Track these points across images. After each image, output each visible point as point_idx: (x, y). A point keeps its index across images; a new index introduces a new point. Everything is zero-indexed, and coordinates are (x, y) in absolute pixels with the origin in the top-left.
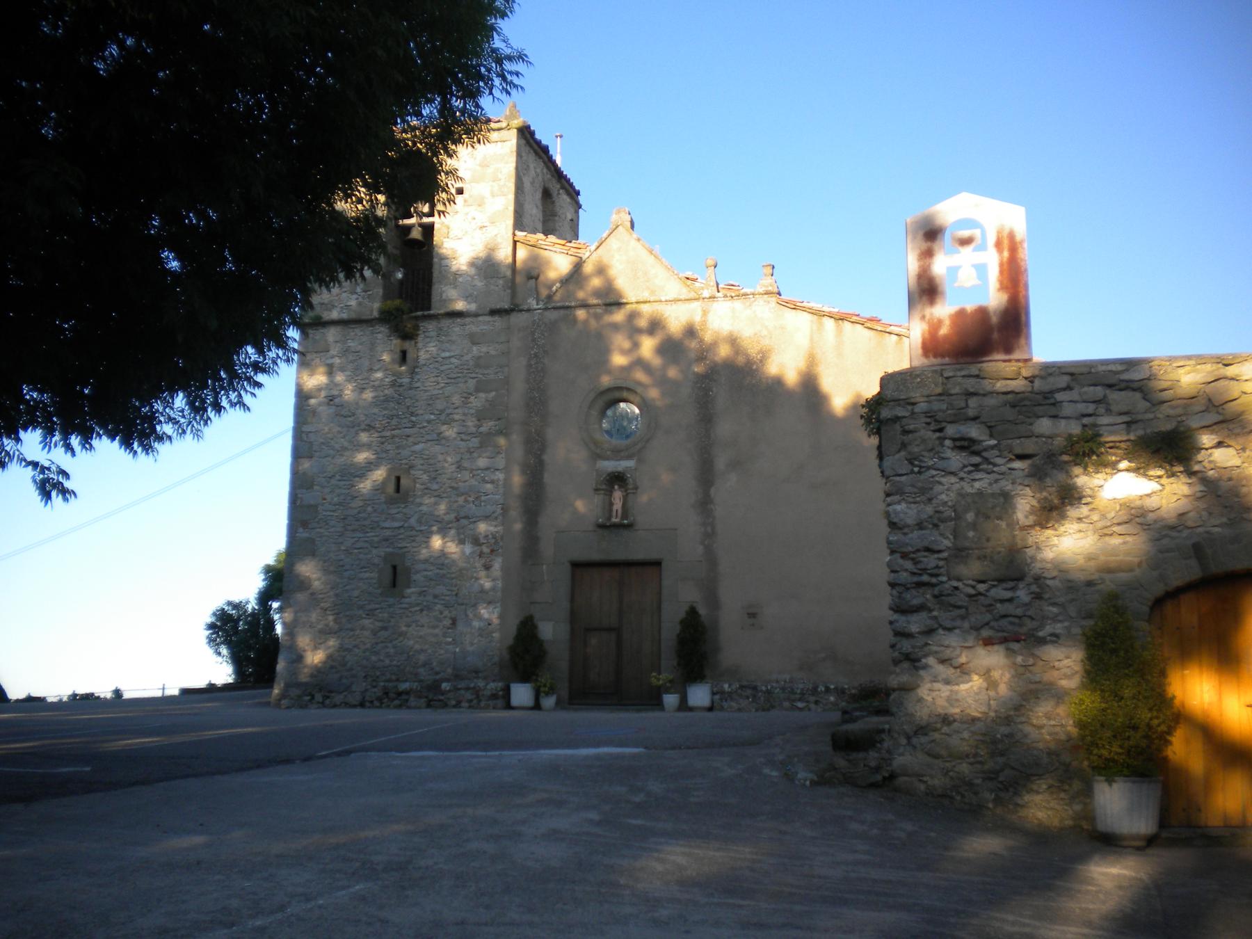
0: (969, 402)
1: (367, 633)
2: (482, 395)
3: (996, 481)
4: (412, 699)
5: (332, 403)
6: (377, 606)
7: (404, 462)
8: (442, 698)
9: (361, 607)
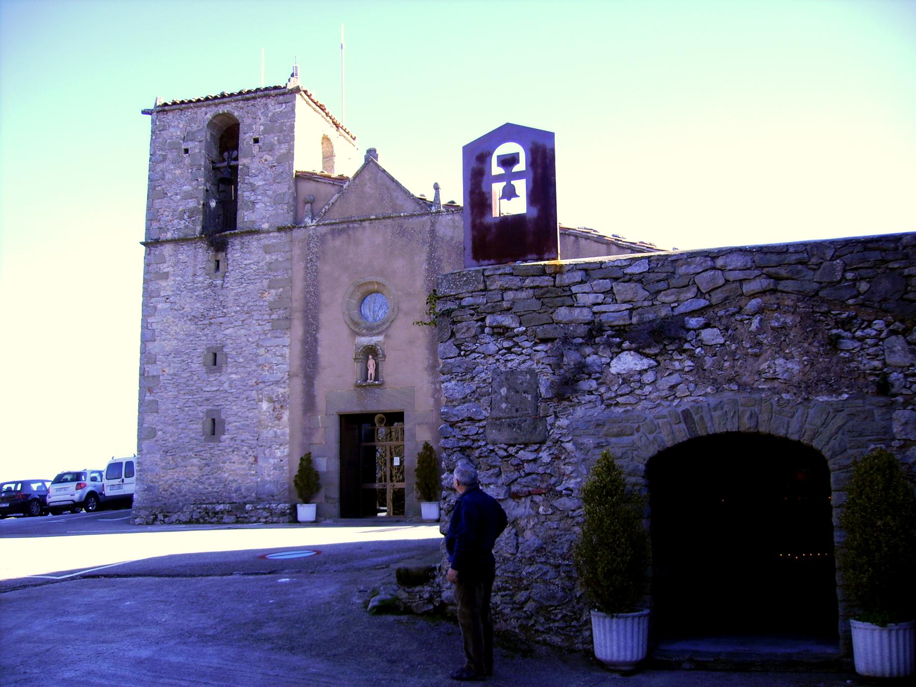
0: (504, 295)
1: (195, 468)
2: (273, 291)
3: (524, 362)
4: (225, 516)
5: (168, 300)
6: (203, 449)
7: (218, 342)
8: (246, 515)
9: (190, 450)
